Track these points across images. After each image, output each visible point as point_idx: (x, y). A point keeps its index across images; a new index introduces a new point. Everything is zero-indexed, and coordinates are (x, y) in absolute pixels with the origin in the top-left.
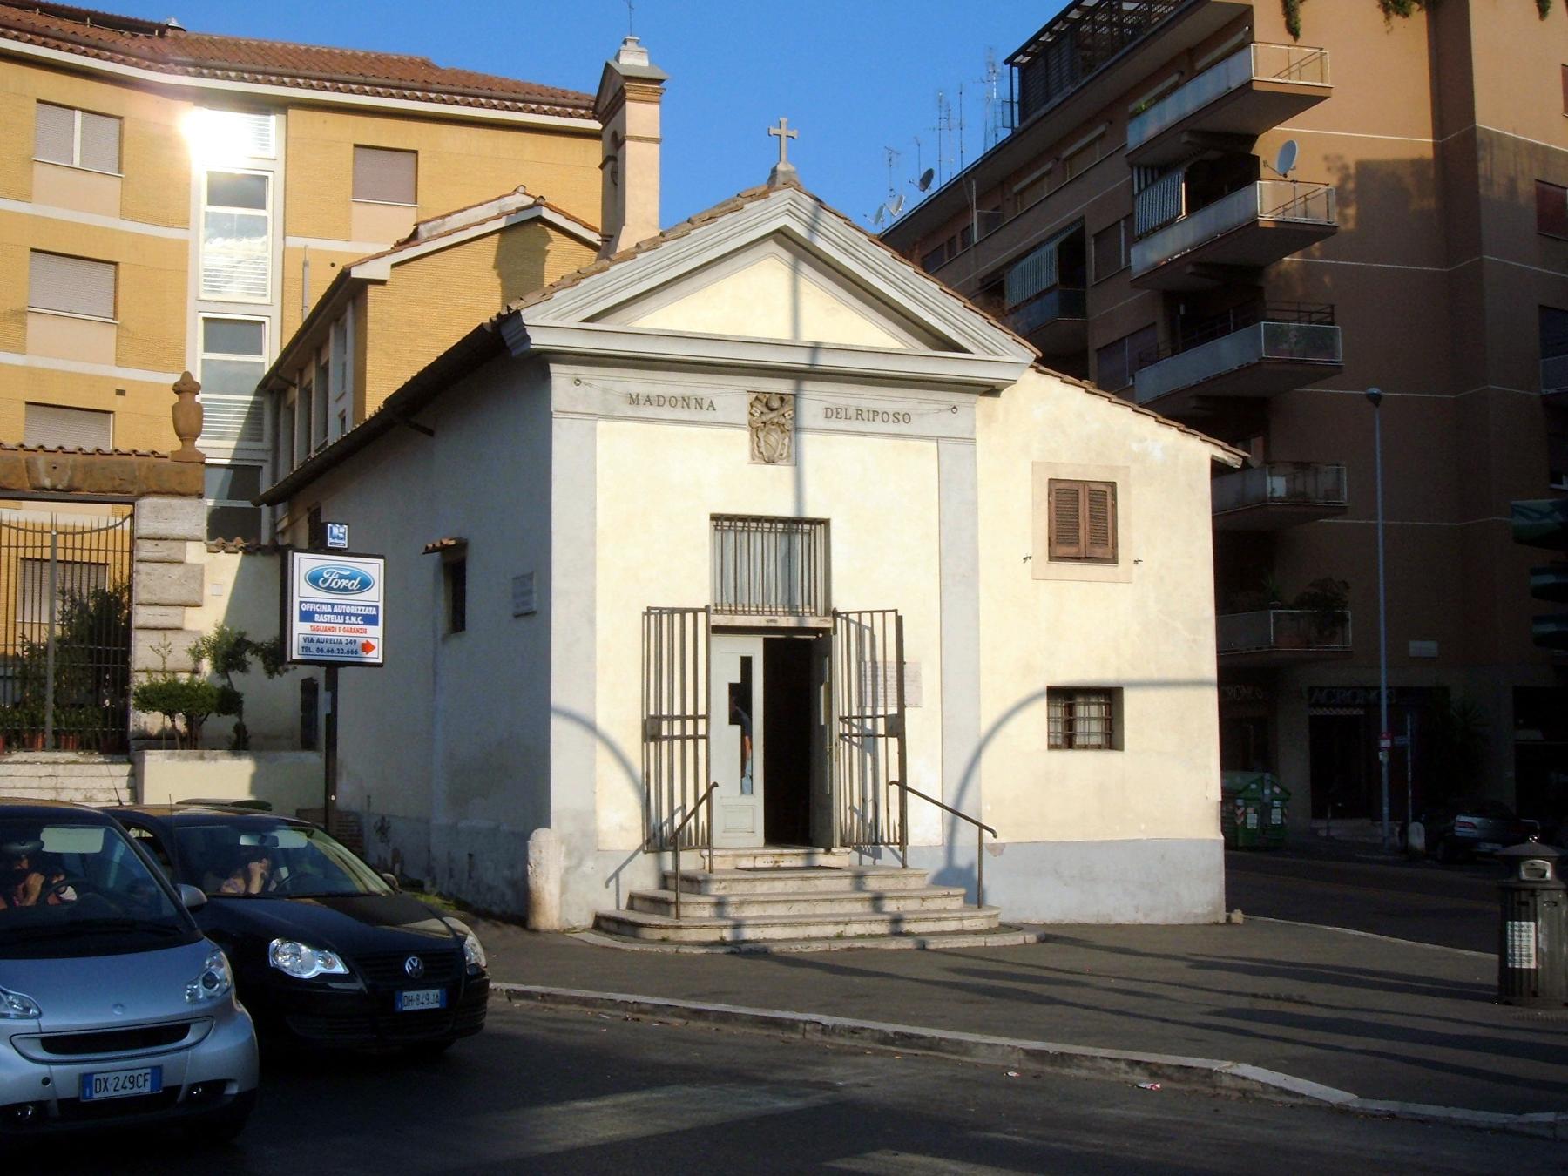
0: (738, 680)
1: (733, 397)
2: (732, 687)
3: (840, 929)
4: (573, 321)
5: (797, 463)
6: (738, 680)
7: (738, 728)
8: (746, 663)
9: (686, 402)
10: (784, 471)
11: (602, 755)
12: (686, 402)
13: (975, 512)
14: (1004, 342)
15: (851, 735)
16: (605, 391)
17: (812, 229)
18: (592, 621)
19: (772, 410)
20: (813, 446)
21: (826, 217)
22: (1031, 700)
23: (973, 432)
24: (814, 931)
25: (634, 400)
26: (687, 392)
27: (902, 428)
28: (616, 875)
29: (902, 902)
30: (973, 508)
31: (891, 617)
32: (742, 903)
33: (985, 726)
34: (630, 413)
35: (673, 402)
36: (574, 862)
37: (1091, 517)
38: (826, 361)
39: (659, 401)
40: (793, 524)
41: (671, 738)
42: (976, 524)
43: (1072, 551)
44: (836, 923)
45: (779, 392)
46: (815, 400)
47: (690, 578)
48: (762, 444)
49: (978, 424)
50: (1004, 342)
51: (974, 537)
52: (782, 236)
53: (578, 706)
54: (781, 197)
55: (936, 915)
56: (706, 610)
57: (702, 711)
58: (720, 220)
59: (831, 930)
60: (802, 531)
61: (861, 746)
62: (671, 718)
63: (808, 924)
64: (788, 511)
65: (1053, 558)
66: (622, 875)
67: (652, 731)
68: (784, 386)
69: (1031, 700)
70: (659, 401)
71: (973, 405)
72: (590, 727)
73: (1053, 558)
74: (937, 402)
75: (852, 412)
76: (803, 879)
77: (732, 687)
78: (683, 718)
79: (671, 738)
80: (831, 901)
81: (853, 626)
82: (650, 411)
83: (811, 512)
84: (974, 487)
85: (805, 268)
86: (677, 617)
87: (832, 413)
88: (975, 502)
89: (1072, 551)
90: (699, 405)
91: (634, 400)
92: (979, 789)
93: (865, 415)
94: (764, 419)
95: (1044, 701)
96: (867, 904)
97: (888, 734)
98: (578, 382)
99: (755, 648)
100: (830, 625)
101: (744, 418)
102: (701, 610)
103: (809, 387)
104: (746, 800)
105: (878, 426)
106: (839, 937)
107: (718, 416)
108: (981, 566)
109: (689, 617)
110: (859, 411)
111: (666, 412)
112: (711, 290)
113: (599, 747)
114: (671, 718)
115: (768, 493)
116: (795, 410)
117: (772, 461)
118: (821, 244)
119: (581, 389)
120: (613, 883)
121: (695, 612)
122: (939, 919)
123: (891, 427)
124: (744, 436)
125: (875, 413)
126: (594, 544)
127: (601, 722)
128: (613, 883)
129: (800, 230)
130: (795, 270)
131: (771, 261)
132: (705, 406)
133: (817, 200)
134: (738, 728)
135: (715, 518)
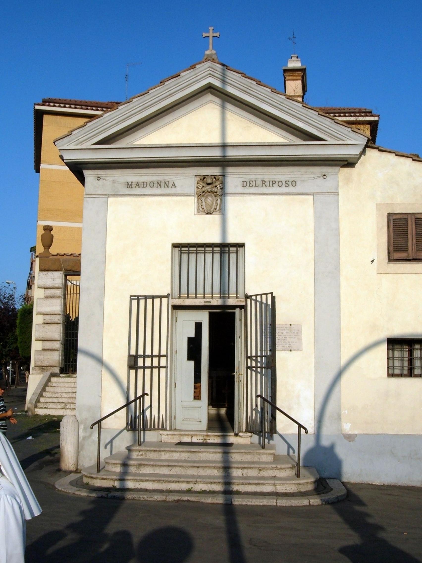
0: (193, 335)
1: (187, 179)
2: (190, 339)
3: (190, 486)
4: (88, 145)
5: (222, 211)
6: (193, 335)
7: (192, 363)
8: (198, 326)
9: (159, 184)
10: (216, 218)
11: (106, 376)
12: (159, 184)
13: (338, 235)
14: (346, 132)
15: (256, 367)
16: (114, 182)
17: (224, 82)
18: (102, 304)
19: (208, 184)
20: (233, 204)
21: (230, 74)
22: (376, 344)
23: (337, 188)
24: (173, 486)
25: (129, 185)
26: (160, 178)
27: (291, 189)
28: (111, 442)
29: (245, 471)
30: (337, 234)
31: (269, 296)
32: (140, 465)
33: (343, 361)
34: (127, 193)
35: (152, 185)
36: (88, 434)
37: (417, 234)
38: (232, 153)
39: (144, 185)
40: (224, 248)
41: (144, 368)
42: (338, 242)
43: (403, 255)
44: (188, 482)
45: (213, 172)
46: (235, 178)
47: (158, 277)
48: (204, 203)
49: (340, 184)
50: (346, 132)
51: (337, 250)
52: (209, 89)
53: (94, 350)
54: (203, 68)
55: (256, 482)
56: (167, 296)
57: (163, 352)
58: (166, 83)
59: (184, 487)
60: (227, 250)
61: (261, 373)
62: (144, 356)
63: (170, 482)
64: (217, 240)
65: (390, 260)
66: (114, 442)
67: (133, 364)
68: (216, 171)
69: (376, 344)
70: (144, 185)
71: (337, 173)
72: (100, 361)
73: (390, 260)
74: (313, 173)
75: (259, 183)
76: (190, 452)
77: (190, 339)
78: (159, 356)
79: (144, 368)
80: (198, 467)
81: (258, 303)
82: (138, 191)
83: (231, 240)
84: (337, 220)
85: (229, 106)
86: (149, 301)
87: (245, 184)
88: (338, 229)
89: (403, 255)
90: (167, 185)
91: (129, 185)
92: (339, 400)
93: (267, 184)
94: (203, 189)
95: (384, 347)
96: (221, 470)
97: (6, 374)
98: (99, 178)
99: (204, 318)
100: (244, 304)
101: (193, 190)
102: (164, 297)
103: (230, 170)
104: (197, 402)
105: (276, 189)
106: (189, 491)
107: (178, 190)
108: (342, 267)
109: (142, 302)
110: (263, 182)
111: (148, 191)
112: (175, 124)
113: (104, 372)
114: (152, 356)
115: (207, 230)
116: (223, 183)
117: (209, 213)
118: (230, 90)
119: (100, 182)
120: (109, 447)
121: (161, 297)
122: (259, 484)
123: (284, 189)
124: (192, 201)
125: (274, 182)
126: (105, 263)
127: (105, 358)
128: (109, 447)
129: (217, 83)
130: (223, 107)
131: (211, 105)
132: (170, 185)
133: (223, 65)
134: (192, 363)
135: (175, 246)
